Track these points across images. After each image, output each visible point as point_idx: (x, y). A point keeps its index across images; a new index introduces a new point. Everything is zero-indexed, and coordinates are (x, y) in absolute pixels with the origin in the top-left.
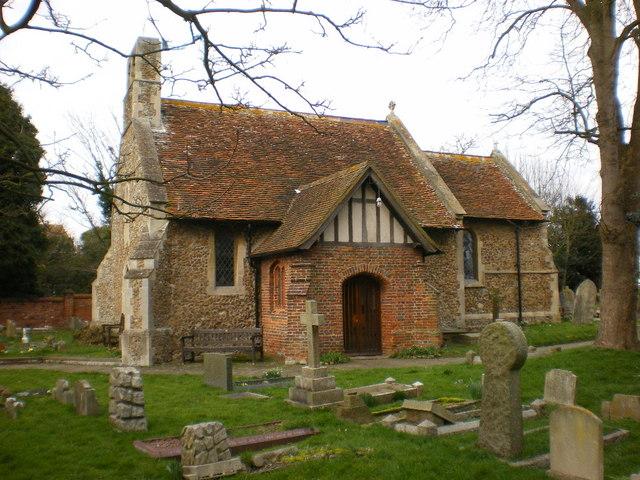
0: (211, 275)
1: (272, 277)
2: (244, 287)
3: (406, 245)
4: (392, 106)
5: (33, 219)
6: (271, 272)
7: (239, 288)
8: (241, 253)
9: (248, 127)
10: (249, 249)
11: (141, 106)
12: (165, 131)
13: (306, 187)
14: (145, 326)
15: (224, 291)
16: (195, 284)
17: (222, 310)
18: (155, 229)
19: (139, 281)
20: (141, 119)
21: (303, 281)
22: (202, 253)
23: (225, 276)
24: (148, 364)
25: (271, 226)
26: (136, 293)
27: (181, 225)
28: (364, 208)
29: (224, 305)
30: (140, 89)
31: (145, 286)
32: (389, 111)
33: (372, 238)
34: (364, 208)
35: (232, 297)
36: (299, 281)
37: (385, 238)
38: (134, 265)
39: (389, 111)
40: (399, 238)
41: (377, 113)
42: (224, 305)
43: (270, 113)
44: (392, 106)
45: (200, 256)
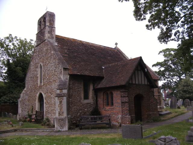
0: (82, 96)
1: (103, 96)
2: (92, 100)
3: (148, 85)
4: (116, 44)
5: (136, 8)
6: (103, 94)
7: (91, 100)
8: (91, 88)
9: (80, 46)
10: (94, 86)
11: (49, 35)
12: (57, 44)
13: (108, 65)
14: (65, 115)
15: (86, 101)
16: (78, 99)
17: (86, 108)
18: (65, 78)
19: (62, 98)
20: (49, 39)
21: (125, 97)
22: (80, 88)
23: (86, 97)
24: (67, 129)
25: (101, 78)
26: (61, 102)
27: (73, 77)
28: (138, 72)
29: (87, 106)
30: (49, 29)
31: (65, 100)
32: (115, 46)
33: (140, 83)
34: (138, 72)
35: (89, 103)
36: (124, 97)
37: (143, 83)
38: (58, 92)
39: (115, 46)
40: (146, 83)
41: (113, 46)
42: (87, 106)
43: (85, 42)
44: (116, 44)
45: (79, 89)
